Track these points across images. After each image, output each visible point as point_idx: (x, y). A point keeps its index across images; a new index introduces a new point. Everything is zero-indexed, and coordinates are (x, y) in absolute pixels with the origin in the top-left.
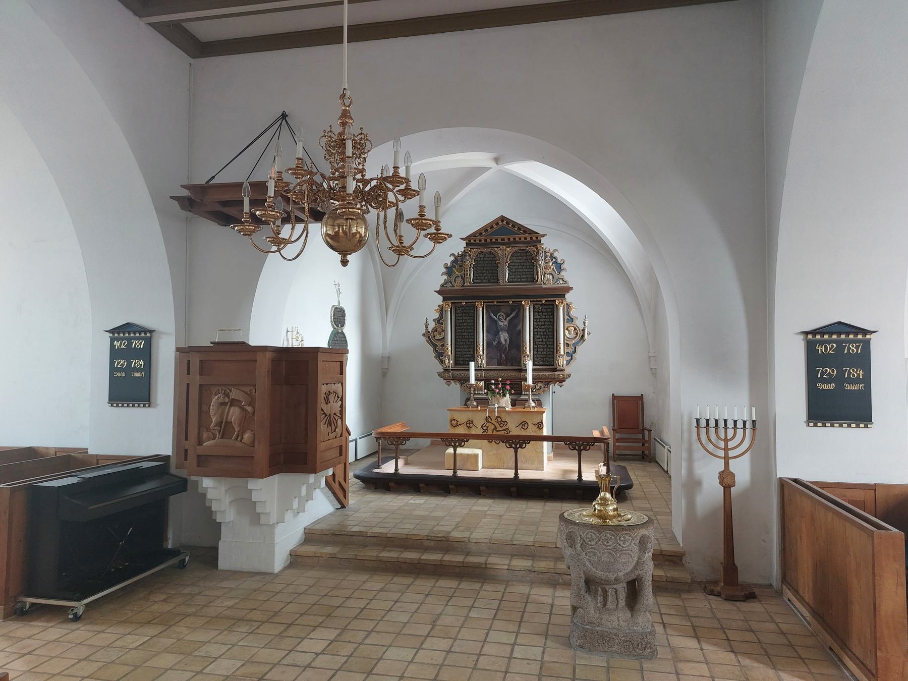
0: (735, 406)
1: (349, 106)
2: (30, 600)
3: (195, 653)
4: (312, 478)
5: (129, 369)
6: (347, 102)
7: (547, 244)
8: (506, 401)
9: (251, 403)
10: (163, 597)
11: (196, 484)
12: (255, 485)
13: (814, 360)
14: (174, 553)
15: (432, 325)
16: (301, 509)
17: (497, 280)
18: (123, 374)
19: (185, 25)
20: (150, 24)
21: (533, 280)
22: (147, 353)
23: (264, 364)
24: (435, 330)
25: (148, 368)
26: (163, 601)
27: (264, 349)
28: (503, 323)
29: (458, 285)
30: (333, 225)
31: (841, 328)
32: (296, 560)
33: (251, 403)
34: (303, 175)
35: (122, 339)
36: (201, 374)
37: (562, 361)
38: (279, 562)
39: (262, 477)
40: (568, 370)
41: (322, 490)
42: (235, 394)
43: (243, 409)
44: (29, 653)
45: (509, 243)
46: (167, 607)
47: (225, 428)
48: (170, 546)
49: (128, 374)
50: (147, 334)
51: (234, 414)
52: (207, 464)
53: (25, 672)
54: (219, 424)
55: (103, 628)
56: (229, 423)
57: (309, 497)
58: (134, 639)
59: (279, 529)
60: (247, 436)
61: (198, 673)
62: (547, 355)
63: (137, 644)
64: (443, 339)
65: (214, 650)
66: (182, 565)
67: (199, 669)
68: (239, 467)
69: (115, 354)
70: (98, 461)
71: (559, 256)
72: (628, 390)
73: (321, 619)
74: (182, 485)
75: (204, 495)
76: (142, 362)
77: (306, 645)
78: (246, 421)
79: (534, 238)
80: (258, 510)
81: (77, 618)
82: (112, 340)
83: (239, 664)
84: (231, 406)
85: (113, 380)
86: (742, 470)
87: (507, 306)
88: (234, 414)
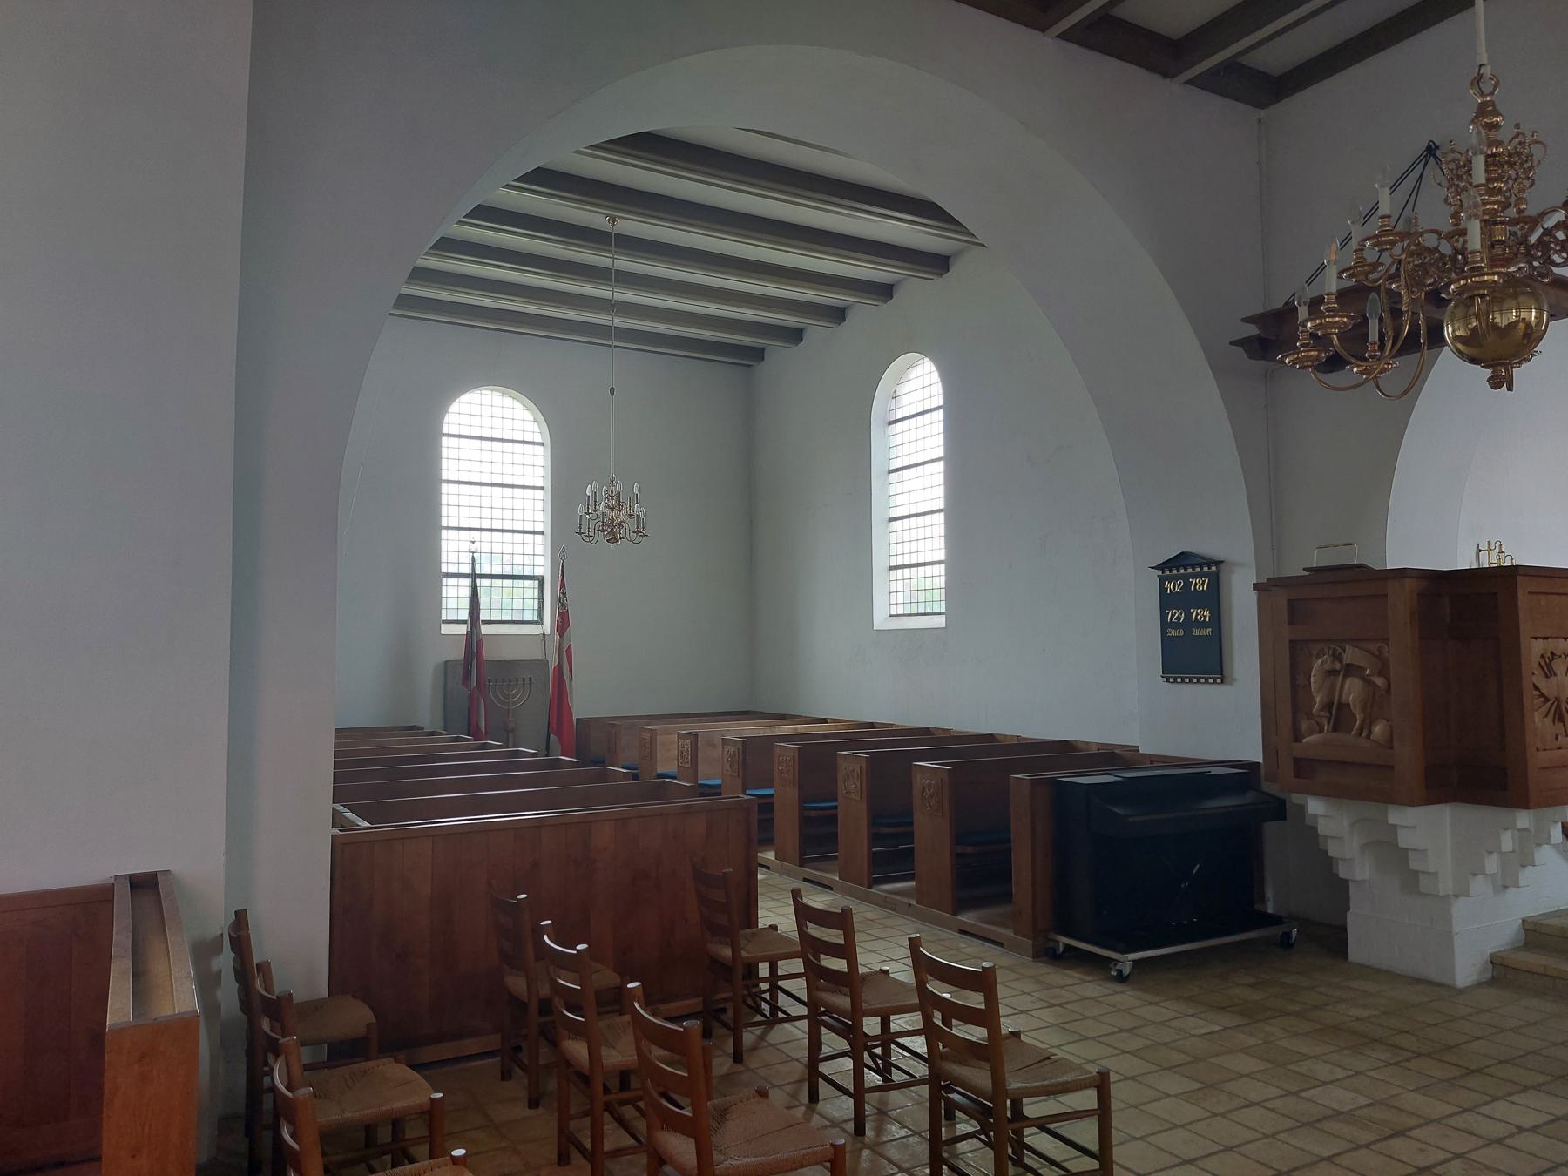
1: (1492, 94)
2: (1064, 940)
3: (1292, 1067)
4: (1524, 819)
5: (1188, 624)
6: (1487, 88)
9: (1383, 671)
10: (1252, 980)
11: (1302, 808)
12: (1399, 816)
14: (1275, 920)
16: (1506, 883)
18: (1180, 633)
19: (1245, 60)
20: (1189, 82)
22: (1213, 598)
23: (1400, 605)
25: (1217, 621)
26: (1250, 986)
27: (1402, 573)
30: (1466, 317)
32: (1501, 972)
33: (1383, 671)
34: (1393, 243)
35: (1176, 578)
36: (1291, 622)
38: (1466, 969)
39: (1412, 804)
41: (1556, 846)
42: (1351, 655)
43: (1367, 682)
44: (1060, 1005)
46: (1256, 996)
47: (1339, 715)
48: (1270, 911)
49: (1188, 633)
50: (1212, 567)
51: (1352, 690)
52: (1307, 770)
53: (1053, 1025)
54: (1328, 706)
55: (1157, 999)
56: (1343, 706)
57: (1526, 861)
58: (1200, 1025)
59: (1459, 908)
60: (1378, 729)
61: (1290, 1093)
63: (1203, 1031)
65: (1323, 1071)
66: (1286, 943)
67: (1294, 1089)
68: (1370, 783)
69: (1167, 601)
70: (1154, 760)
73: (1541, 1079)
74: (1278, 810)
75: (1315, 829)
76: (1207, 613)
77: (1499, 1109)
78: (1375, 702)
80: (1413, 865)
81: (1121, 978)
82: (1162, 581)
83: (1363, 1101)
84: (1346, 676)
85: (1166, 641)
88: (1352, 690)
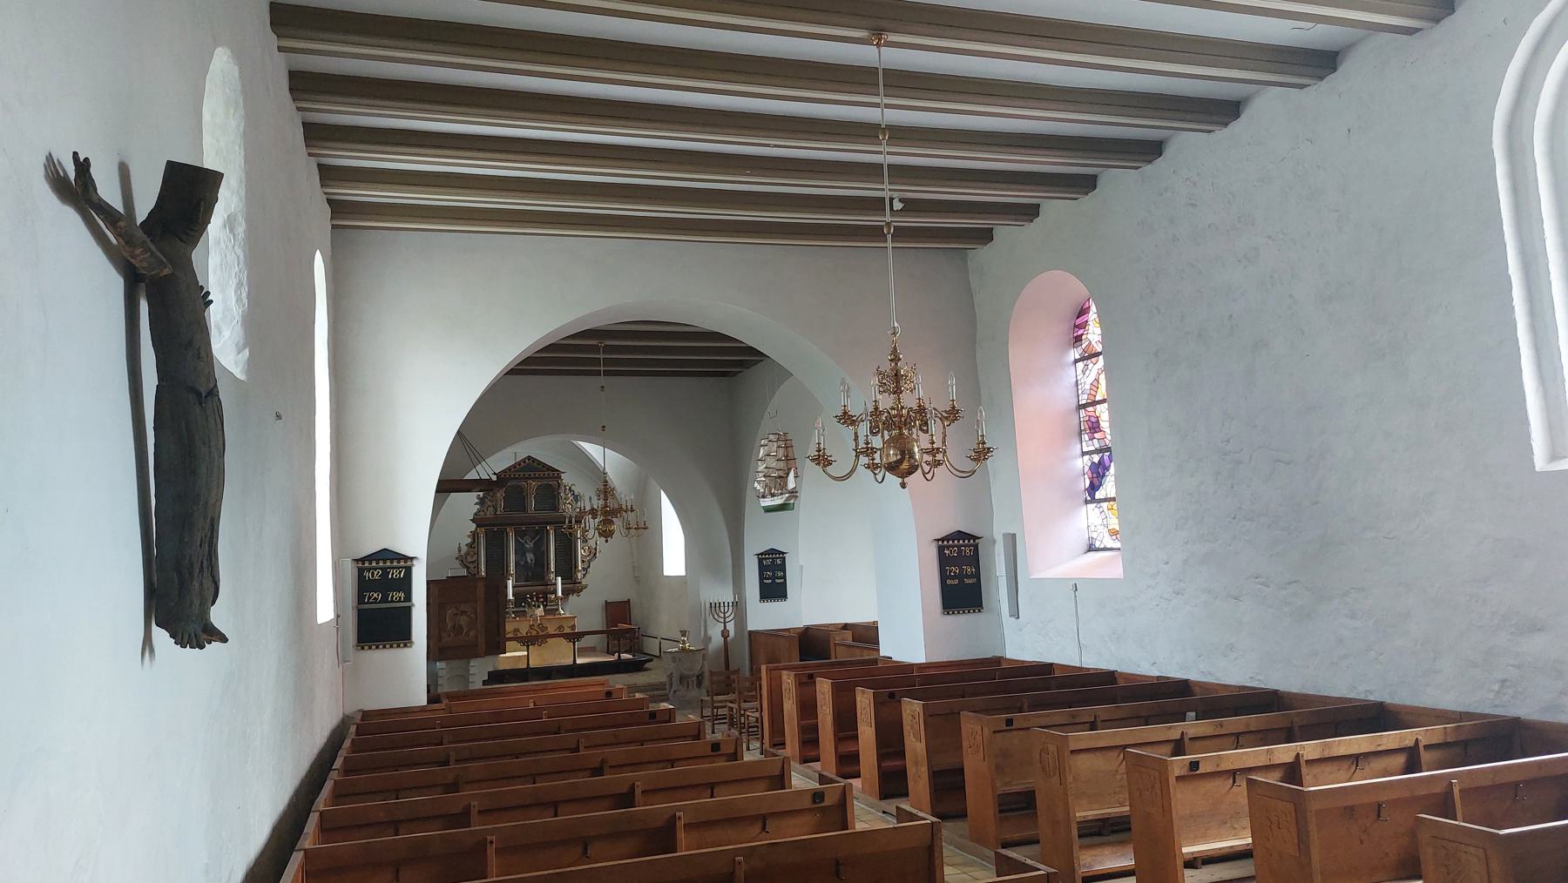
0: (726, 595)
7: (566, 479)
8: (540, 611)
13: (762, 569)
15: (464, 549)
17: (524, 509)
21: (555, 508)
24: (467, 554)
28: (530, 545)
29: (490, 513)
31: (773, 551)
37: (579, 575)
40: (584, 582)
45: (534, 479)
47: (458, 629)
49: (962, 581)
62: (568, 569)
64: (478, 561)
71: (576, 490)
72: (617, 596)
79: (555, 474)
86: (731, 627)
87: (534, 531)
88: (463, 620)
